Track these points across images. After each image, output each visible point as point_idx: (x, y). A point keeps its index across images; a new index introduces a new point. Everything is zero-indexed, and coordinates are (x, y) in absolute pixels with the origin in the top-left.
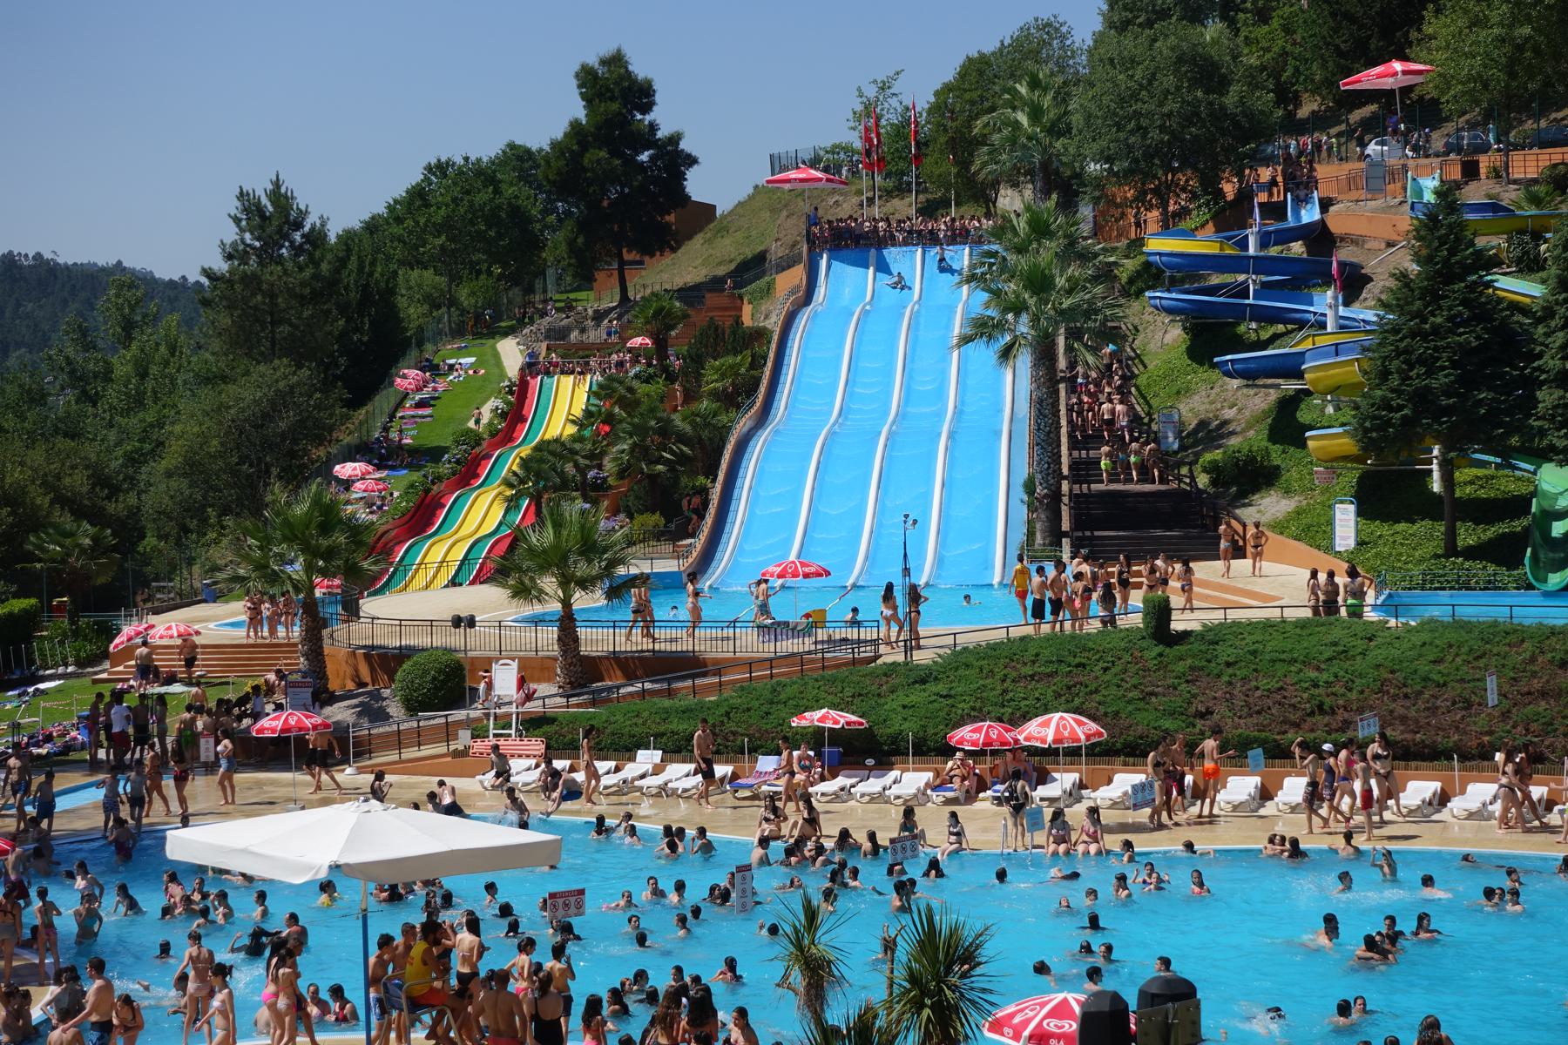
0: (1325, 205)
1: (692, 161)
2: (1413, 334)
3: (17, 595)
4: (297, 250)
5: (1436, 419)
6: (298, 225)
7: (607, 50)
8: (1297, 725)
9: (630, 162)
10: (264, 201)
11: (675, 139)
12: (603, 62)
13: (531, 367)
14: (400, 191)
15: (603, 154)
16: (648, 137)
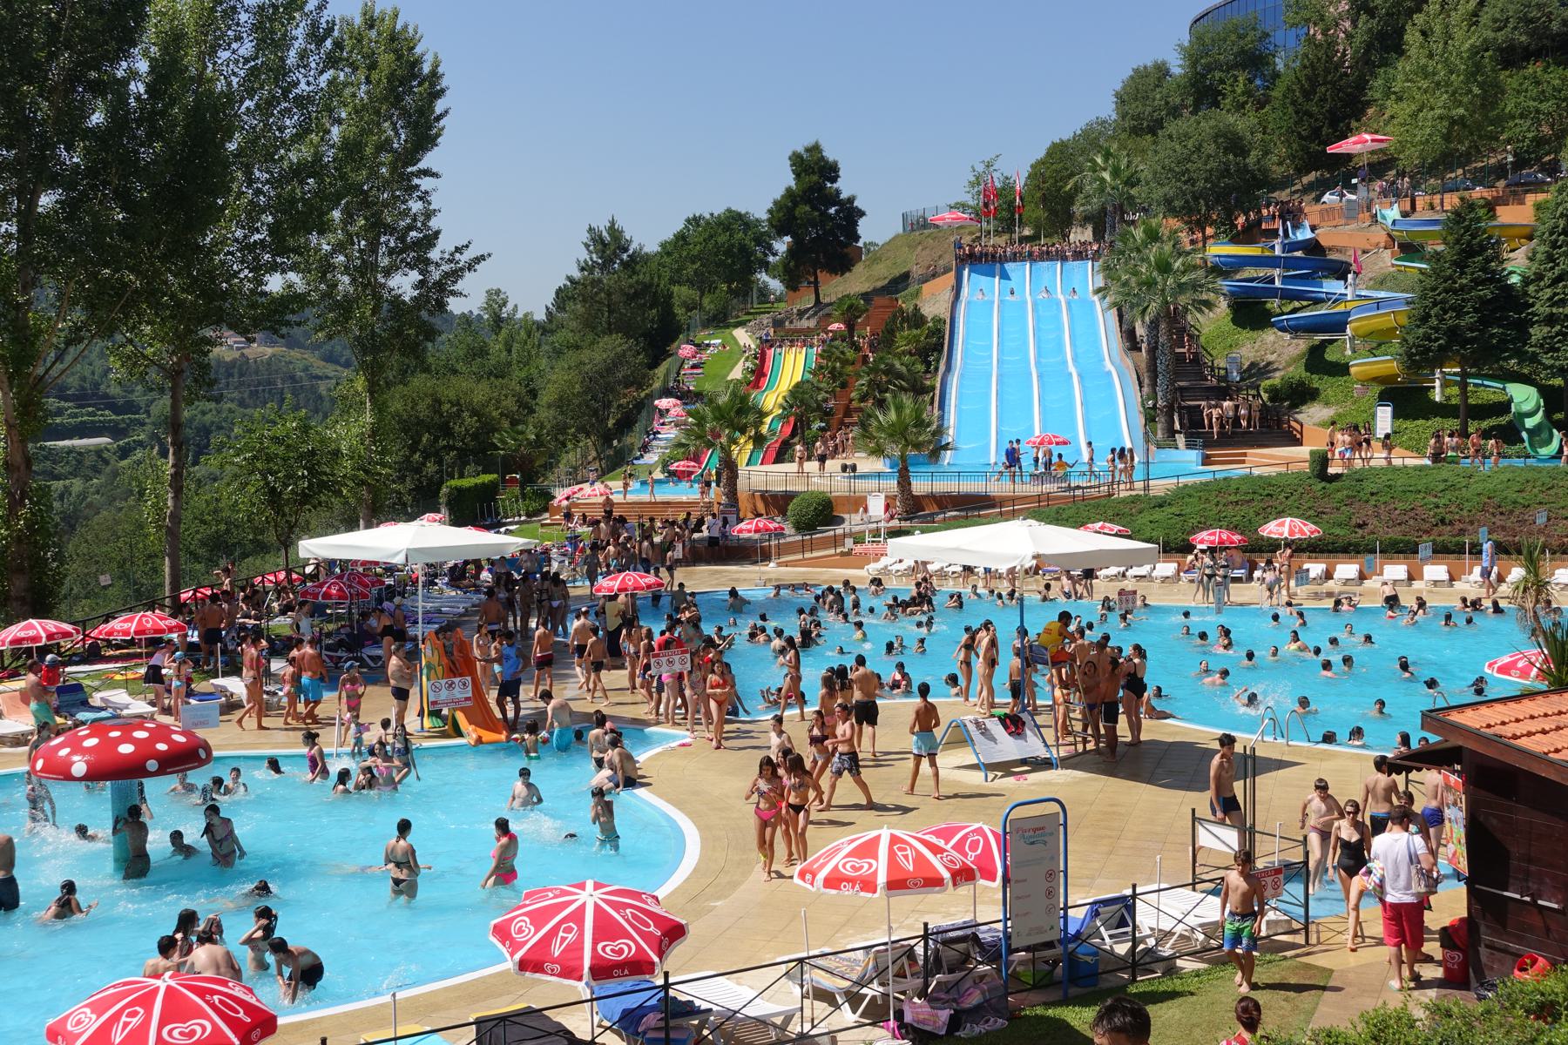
0: (1313, 228)
1: (862, 214)
2: (1446, 291)
3: (484, 472)
4: (624, 264)
5: (1463, 347)
6: (626, 250)
7: (809, 142)
8: (1426, 532)
9: (824, 214)
10: (605, 234)
11: (851, 200)
12: (807, 150)
13: (766, 343)
14: (669, 235)
15: (808, 208)
16: (834, 198)
